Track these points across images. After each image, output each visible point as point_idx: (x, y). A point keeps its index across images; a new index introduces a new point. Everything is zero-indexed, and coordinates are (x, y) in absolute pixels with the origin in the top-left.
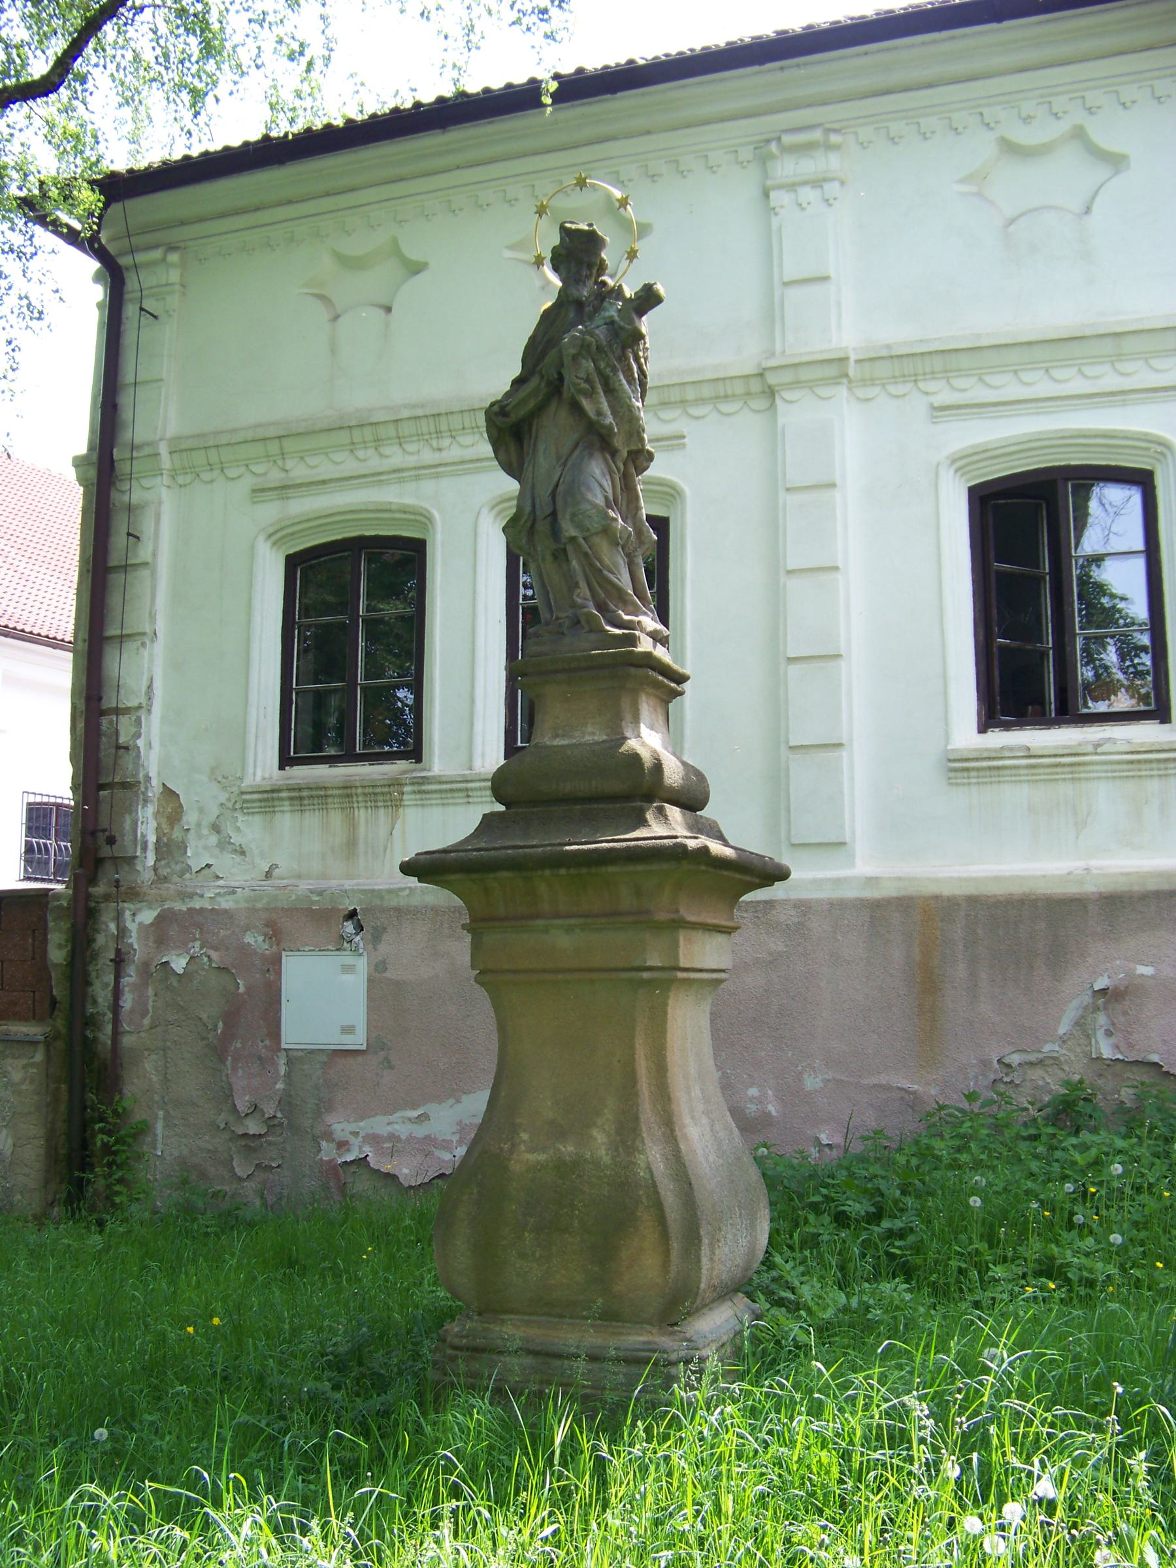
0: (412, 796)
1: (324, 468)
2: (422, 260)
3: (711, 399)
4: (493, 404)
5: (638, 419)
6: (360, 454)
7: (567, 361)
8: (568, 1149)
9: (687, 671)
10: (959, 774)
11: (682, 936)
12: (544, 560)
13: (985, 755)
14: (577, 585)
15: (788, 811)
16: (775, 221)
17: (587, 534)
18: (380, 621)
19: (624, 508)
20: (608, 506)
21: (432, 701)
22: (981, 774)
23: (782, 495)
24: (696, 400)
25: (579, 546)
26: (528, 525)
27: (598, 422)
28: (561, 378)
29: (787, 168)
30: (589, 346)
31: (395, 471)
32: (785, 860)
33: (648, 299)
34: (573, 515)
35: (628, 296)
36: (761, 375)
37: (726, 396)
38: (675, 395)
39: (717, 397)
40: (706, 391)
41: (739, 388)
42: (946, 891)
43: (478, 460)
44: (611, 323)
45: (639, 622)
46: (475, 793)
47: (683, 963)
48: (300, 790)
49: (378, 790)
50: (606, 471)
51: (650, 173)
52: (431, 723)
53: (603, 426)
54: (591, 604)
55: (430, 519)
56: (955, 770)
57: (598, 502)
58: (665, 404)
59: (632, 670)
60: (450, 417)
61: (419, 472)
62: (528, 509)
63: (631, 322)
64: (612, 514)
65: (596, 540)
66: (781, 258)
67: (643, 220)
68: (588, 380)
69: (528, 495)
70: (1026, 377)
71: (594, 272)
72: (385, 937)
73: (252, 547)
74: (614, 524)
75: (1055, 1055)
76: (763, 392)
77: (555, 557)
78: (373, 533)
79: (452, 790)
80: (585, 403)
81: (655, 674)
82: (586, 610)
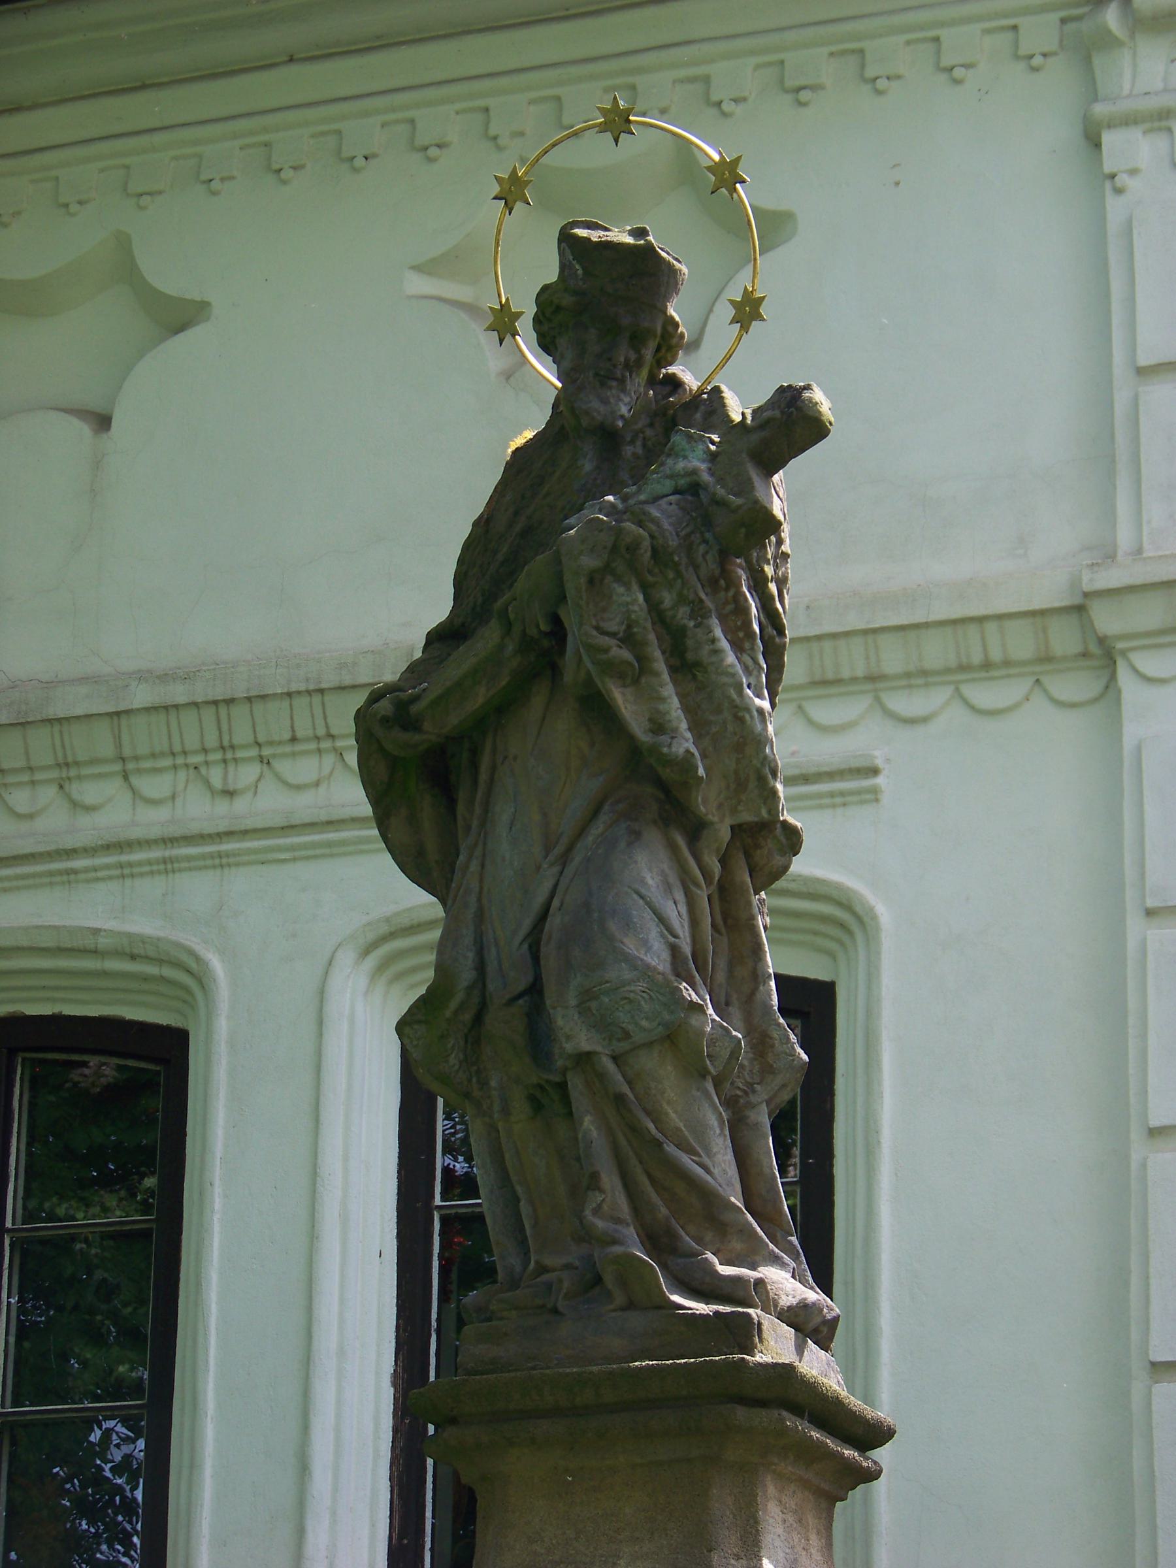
2: (193, 294)
3: (948, 671)
4: (376, 696)
5: (761, 741)
7: (574, 585)
9: (882, 1412)
12: (506, 1111)
14: (594, 1183)
16: (1116, 209)
17: (625, 1046)
18: (63, 1244)
19: (721, 977)
20: (680, 971)
21: (194, 1465)
23: (1134, 923)
24: (908, 675)
25: (602, 1076)
26: (468, 1017)
27: (654, 750)
28: (558, 631)
30: (633, 548)
31: (108, 847)
33: (789, 425)
34: (587, 996)
35: (737, 418)
36: (1079, 609)
37: (987, 665)
38: (853, 660)
39: (963, 668)
40: (936, 651)
41: (1021, 643)
43: (330, 824)
44: (692, 488)
45: (760, 1283)
50: (673, 879)
51: (790, 83)
52: (189, 1526)
53: (669, 762)
54: (630, 1232)
55: (201, 976)
57: (653, 962)
58: (824, 683)
59: (741, 1414)
60: (258, 708)
61: (175, 850)
62: (466, 976)
63: (744, 487)
64: (691, 995)
65: (648, 1062)
67: (769, 204)
68: (628, 639)
69: (468, 938)
71: (648, 354)
74: (695, 1021)
76: (1085, 655)
77: (536, 1106)
78: (46, 1010)
80: (622, 700)
81: (801, 1425)
82: (617, 1249)
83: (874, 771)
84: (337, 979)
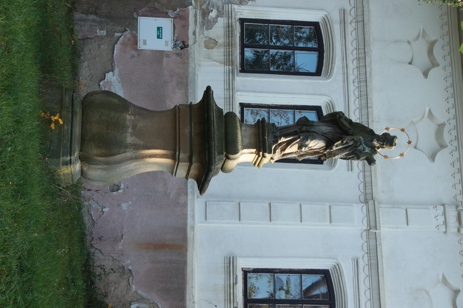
0: (228, 69)
1: (350, 38)
6: (355, 52)
8: (130, 130)
10: (228, 260)
11: (188, 164)
13: (234, 269)
15: (218, 201)
22: (228, 268)
29: (452, 214)
30: (357, 144)
32: (204, 195)
39: (365, 183)
40: (368, 179)
42: (189, 254)
46: (228, 92)
47: (180, 164)
48: (232, 27)
49: (230, 57)
55: (328, 78)
56: (230, 259)
66: (417, 208)
68: (346, 143)
70: (368, 293)
72: (178, 58)
73: (322, 10)
75: (131, 289)
79: (229, 84)
83: (352, 171)
84: (326, 97)
